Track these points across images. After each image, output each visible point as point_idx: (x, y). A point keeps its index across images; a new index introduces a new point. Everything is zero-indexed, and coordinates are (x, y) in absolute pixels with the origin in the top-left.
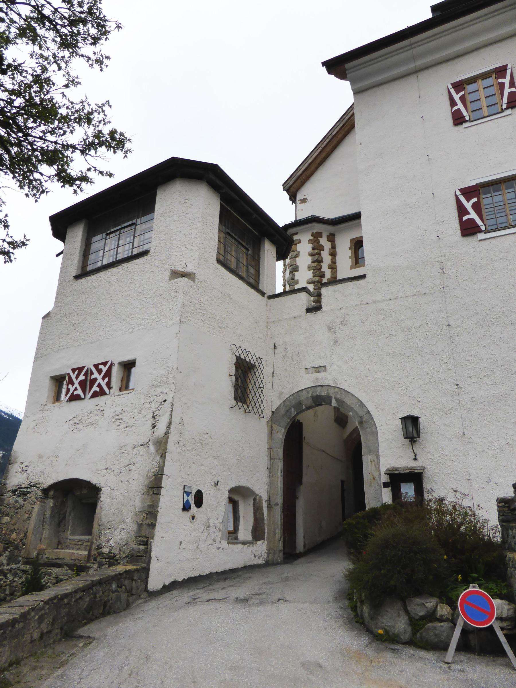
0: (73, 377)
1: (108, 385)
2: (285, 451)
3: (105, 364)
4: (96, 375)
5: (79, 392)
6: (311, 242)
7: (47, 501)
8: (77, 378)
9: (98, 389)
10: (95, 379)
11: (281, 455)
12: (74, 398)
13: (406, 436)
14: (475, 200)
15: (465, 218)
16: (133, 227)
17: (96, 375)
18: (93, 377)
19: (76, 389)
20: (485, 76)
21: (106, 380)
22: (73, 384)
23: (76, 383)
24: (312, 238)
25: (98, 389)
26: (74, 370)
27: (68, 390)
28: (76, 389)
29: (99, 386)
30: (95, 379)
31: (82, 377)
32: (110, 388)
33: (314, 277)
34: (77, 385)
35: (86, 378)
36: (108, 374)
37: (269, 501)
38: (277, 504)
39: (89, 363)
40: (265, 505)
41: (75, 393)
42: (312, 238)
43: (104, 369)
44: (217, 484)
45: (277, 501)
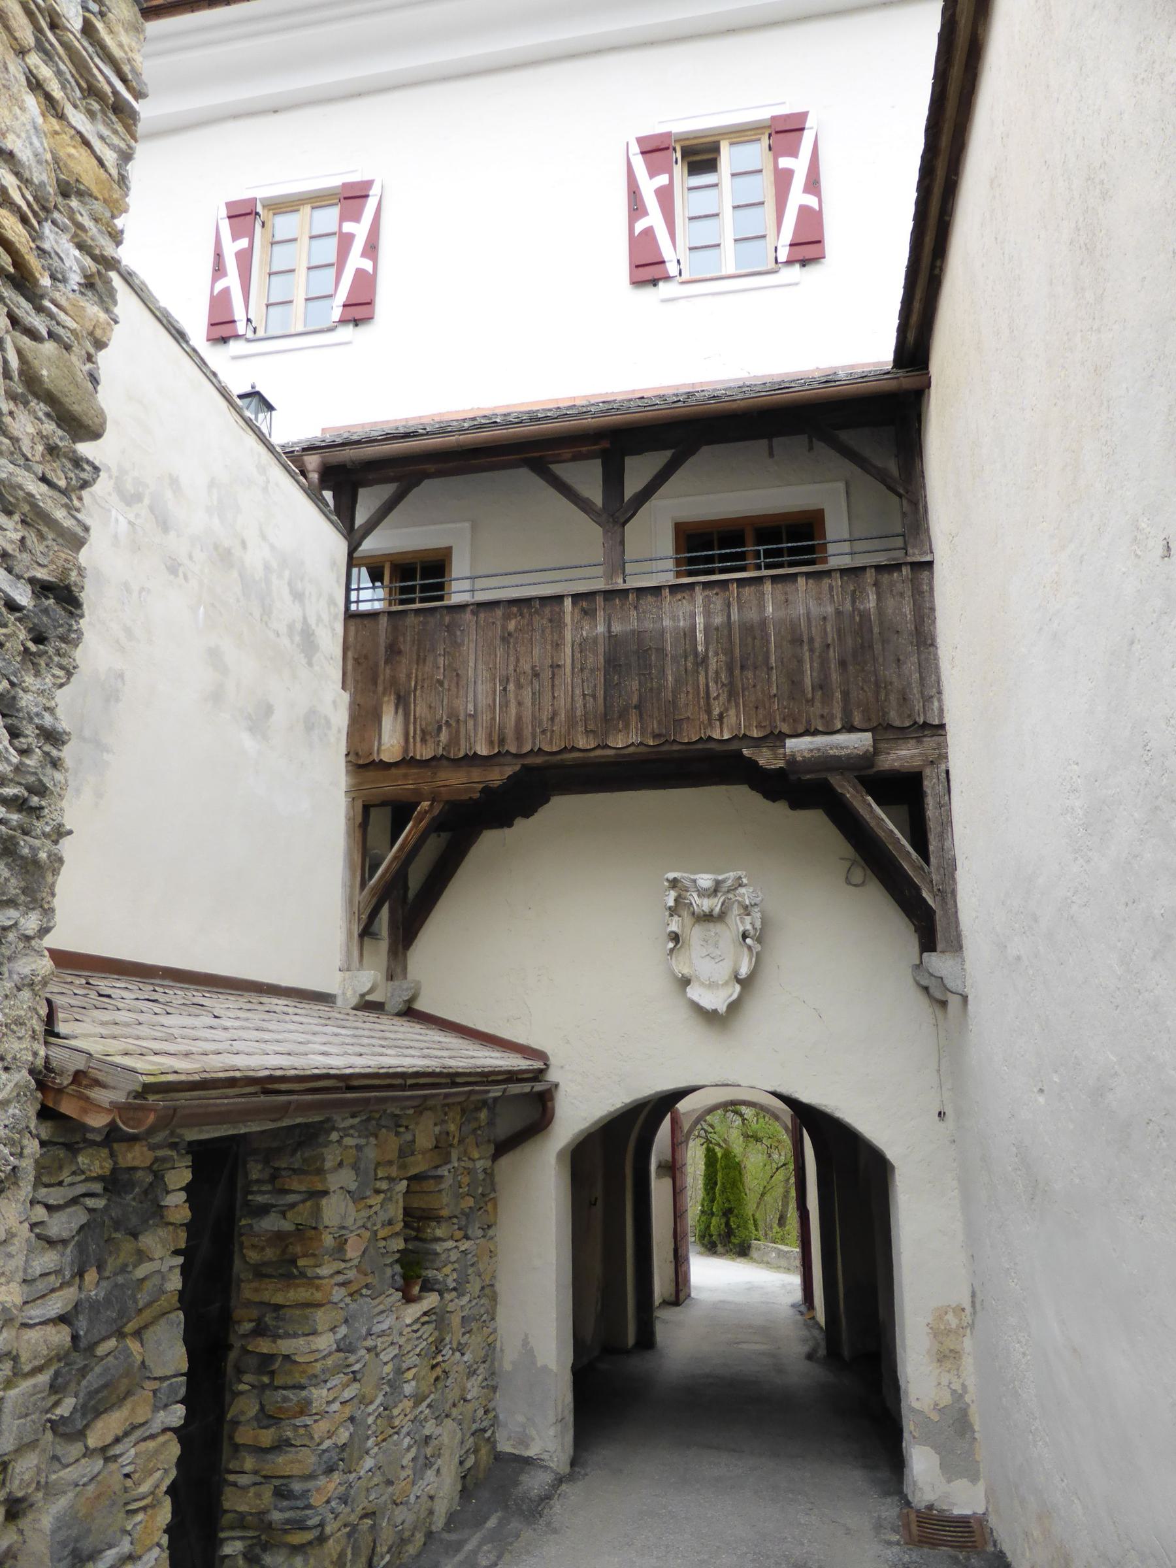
20: (318, 200)
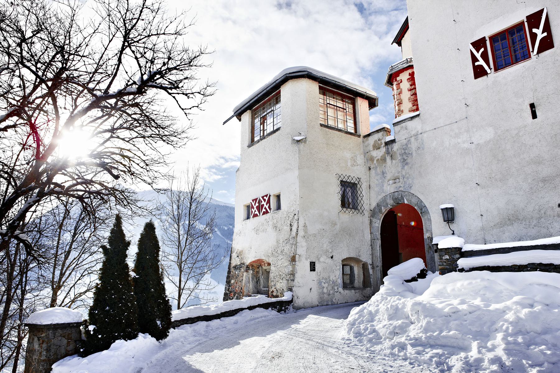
0: (253, 204)
1: (269, 207)
2: (382, 234)
3: (266, 196)
4: (263, 203)
5: (257, 212)
6: (409, 80)
7: (249, 271)
8: (255, 205)
9: (265, 210)
10: (263, 205)
11: (379, 236)
12: (255, 216)
13: (446, 219)
14: (482, 50)
15: (477, 64)
16: (273, 112)
17: (263, 203)
18: (262, 204)
19: (255, 211)
21: (268, 205)
22: (254, 208)
23: (255, 207)
24: (409, 77)
25: (265, 210)
26: (253, 200)
27: (252, 212)
28: (255, 211)
29: (265, 208)
30: (263, 205)
31: (257, 204)
32: (270, 209)
33: (413, 106)
34: (255, 209)
35: (259, 204)
36: (269, 202)
37: (372, 264)
38: (378, 266)
39: (259, 196)
40: (370, 267)
41: (255, 213)
42: (409, 77)
43: (267, 199)
44: (332, 257)
45: (378, 264)
